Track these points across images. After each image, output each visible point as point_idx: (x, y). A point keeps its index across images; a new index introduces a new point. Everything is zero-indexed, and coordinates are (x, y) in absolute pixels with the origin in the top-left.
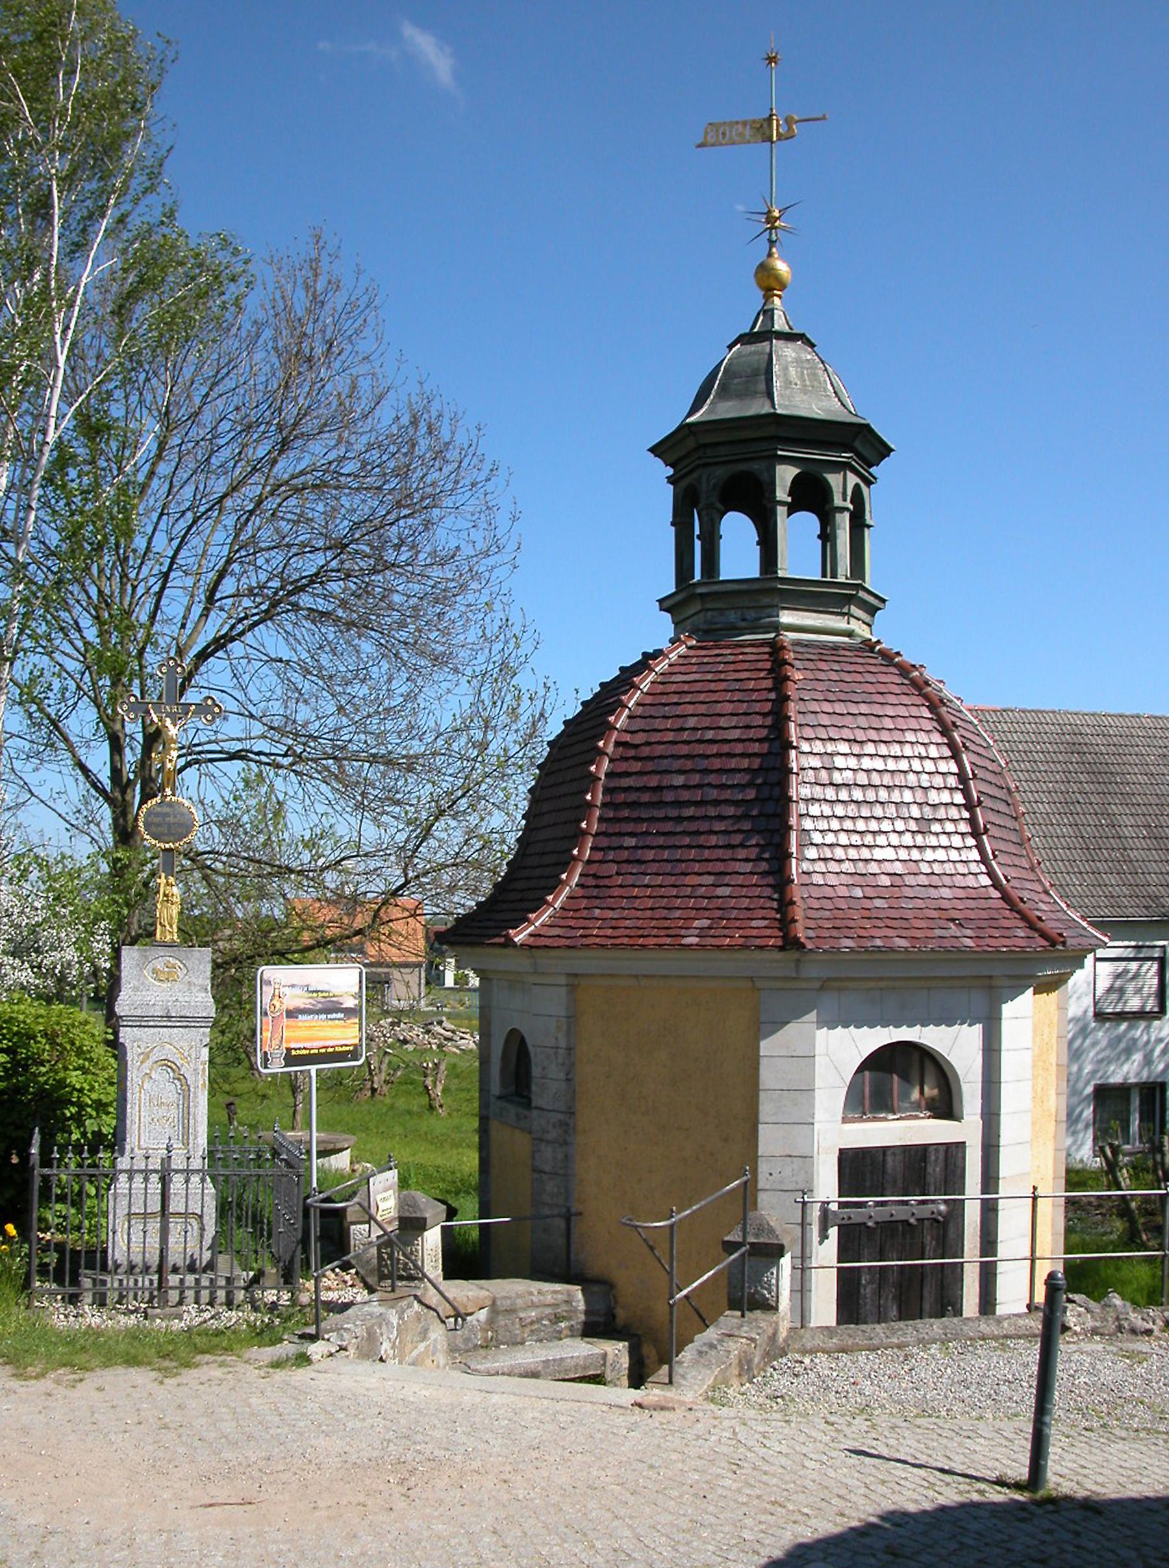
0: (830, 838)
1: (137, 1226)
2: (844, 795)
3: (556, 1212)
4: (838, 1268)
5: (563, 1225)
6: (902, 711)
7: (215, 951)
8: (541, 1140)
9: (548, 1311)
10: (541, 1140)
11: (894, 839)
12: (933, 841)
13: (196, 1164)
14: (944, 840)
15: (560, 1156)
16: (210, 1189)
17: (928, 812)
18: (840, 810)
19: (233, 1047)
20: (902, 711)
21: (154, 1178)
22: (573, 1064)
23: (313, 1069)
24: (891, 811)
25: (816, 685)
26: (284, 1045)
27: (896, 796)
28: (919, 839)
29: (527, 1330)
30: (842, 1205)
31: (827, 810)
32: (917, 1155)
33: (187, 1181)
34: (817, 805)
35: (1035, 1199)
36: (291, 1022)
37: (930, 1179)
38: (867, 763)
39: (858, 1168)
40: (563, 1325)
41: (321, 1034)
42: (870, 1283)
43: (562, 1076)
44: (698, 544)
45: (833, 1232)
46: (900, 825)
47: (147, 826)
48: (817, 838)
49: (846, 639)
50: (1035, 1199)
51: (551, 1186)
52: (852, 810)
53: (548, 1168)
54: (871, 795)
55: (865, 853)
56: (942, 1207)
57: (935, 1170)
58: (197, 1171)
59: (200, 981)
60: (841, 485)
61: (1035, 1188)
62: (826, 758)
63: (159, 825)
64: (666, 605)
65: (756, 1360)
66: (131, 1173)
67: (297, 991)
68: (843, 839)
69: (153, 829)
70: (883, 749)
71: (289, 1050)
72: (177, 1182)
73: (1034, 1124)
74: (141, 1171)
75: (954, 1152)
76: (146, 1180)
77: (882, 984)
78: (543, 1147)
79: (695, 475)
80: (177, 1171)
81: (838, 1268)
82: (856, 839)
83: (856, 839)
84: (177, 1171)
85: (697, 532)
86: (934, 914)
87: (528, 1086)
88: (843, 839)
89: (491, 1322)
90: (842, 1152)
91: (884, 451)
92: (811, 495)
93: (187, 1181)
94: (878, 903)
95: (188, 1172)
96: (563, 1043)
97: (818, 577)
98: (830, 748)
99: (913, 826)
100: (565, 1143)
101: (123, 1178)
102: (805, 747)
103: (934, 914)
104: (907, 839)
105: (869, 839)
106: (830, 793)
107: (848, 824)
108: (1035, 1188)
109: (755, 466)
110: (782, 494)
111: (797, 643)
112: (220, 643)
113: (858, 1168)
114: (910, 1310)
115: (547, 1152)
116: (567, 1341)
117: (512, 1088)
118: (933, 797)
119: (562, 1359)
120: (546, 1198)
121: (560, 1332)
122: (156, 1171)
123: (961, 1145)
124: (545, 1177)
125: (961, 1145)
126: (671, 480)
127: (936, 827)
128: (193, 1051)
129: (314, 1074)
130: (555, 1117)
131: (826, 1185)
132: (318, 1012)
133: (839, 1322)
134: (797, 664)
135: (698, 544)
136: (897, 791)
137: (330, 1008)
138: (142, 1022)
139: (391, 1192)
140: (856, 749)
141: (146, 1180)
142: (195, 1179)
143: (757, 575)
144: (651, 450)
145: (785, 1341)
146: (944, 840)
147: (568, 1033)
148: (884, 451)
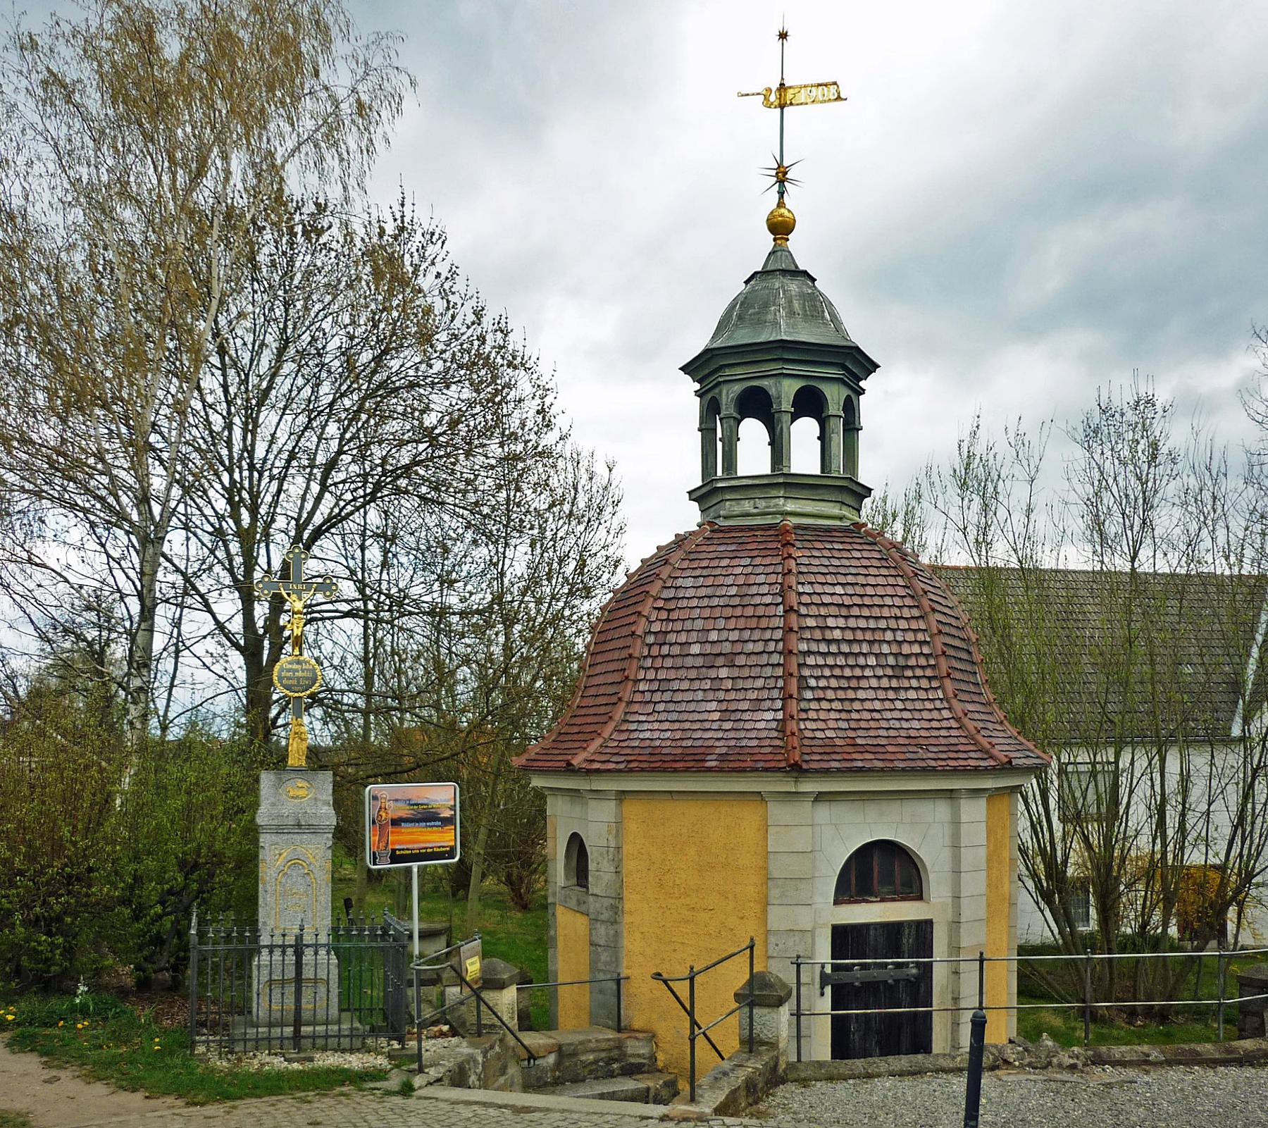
0: (823, 683)
2: (834, 649)
3: (609, 977)
5: (615, 987)
6: (881, 580)
7: (335, 775)
8: (597, 920)
9: (603, 1055)
10: (597, 920)
11: (874, 683)
12: (906, 684)
13: (323, 939)
14: (914, 683)
15: (612, 932)
16: (334, 960)
17: (902, 662)
18: (830, 661)
19: (347, 838)
20: (881, 580)
21: (290, 951)
22: (621, 860)
23: (415, 866)
24: (872, 661)
26: (390, 847)
27: (876, 649)
28: (894, 683)
29: (587, 1070)
30: (835, 968)
31: (821, 661)
32: (893, 930)
33: (316, 954)
34: (812, 657)
35: (981, 961)
36: (396, 829)
38: (852, 623)
39: (846, 939)
40: (615, 1066)
41: (422, 838)
44: (719, 445)
45: (828, 990)
46: (880, 672)
47: (280, 679)
48: (813, 683)
49: (838, 523)
50: (981, 961)
51: (604, 957)
52: (841, 661)
54: (856, 649)
55: (851, 694)
56: (914, 971)
57: (907, 940)
58: (324, 945)
59: (324, 797)
60: (834, 396)
61: (982, 954)
62: (820, 619)
63: (289, 678)
64: (694, 495)
65: (760, 1086)
66: (271, 948)
67: (399, 804)
68: (834, 683)
70: (866, 612)
71: (394, 851)
72: (309, 952)
73: (989, 905)
74: (280, 946)
75: (923, 929)
76: (284, 953)
79: (717, 391)
80: (308, 946)
82: (844, 683)
83: (844, 683)
84: (308, 946)
85: (719, 435)
87: (587, 878)
88: (834, 683)
89: (558, 1064)
91: (870, 367)
92: (809, 403)
93: (316, 954)
95: (316, 946)
96: (613, 844)
97: (818, 472)
98: (823, 611)
99: (889, 672)
100: (616, 922)
101: (265, 952)
102: (803, 610)
104: (885, 683)
105: (854, 683)
106: (823, 648)
107: (837, 672)
108: (982, 954)
109: (764, 383)
110: (787, 406)
111: (798, 527)
112: (333, 521)
113: (846, 939)
114: (890, 1048)
115: (602, 929)
116: (619, 1079)
117: (574, 881)
118: (906, 649)
120: (600, 966)
122: (291, 946)
123: (929, 923)
125: (929, 923)
126: (699, 394)
127: (909, 673)
128: (317, 852)
129: (415, 870)
130: (607, 902)
131: (823, 953)
132: (418, 821)
133: (834, 1057)
134: (798, 544)
135: (719, 445)
136: (876, 645)
137: (428, 817)
139: (476, 958)
140: (844, 612)
141: (284, 953)
142: (322, 952)
143: (769, 472)
145: (784, 1071)
146: (914, 683)
147: (617, 836)
148: (870, 367)
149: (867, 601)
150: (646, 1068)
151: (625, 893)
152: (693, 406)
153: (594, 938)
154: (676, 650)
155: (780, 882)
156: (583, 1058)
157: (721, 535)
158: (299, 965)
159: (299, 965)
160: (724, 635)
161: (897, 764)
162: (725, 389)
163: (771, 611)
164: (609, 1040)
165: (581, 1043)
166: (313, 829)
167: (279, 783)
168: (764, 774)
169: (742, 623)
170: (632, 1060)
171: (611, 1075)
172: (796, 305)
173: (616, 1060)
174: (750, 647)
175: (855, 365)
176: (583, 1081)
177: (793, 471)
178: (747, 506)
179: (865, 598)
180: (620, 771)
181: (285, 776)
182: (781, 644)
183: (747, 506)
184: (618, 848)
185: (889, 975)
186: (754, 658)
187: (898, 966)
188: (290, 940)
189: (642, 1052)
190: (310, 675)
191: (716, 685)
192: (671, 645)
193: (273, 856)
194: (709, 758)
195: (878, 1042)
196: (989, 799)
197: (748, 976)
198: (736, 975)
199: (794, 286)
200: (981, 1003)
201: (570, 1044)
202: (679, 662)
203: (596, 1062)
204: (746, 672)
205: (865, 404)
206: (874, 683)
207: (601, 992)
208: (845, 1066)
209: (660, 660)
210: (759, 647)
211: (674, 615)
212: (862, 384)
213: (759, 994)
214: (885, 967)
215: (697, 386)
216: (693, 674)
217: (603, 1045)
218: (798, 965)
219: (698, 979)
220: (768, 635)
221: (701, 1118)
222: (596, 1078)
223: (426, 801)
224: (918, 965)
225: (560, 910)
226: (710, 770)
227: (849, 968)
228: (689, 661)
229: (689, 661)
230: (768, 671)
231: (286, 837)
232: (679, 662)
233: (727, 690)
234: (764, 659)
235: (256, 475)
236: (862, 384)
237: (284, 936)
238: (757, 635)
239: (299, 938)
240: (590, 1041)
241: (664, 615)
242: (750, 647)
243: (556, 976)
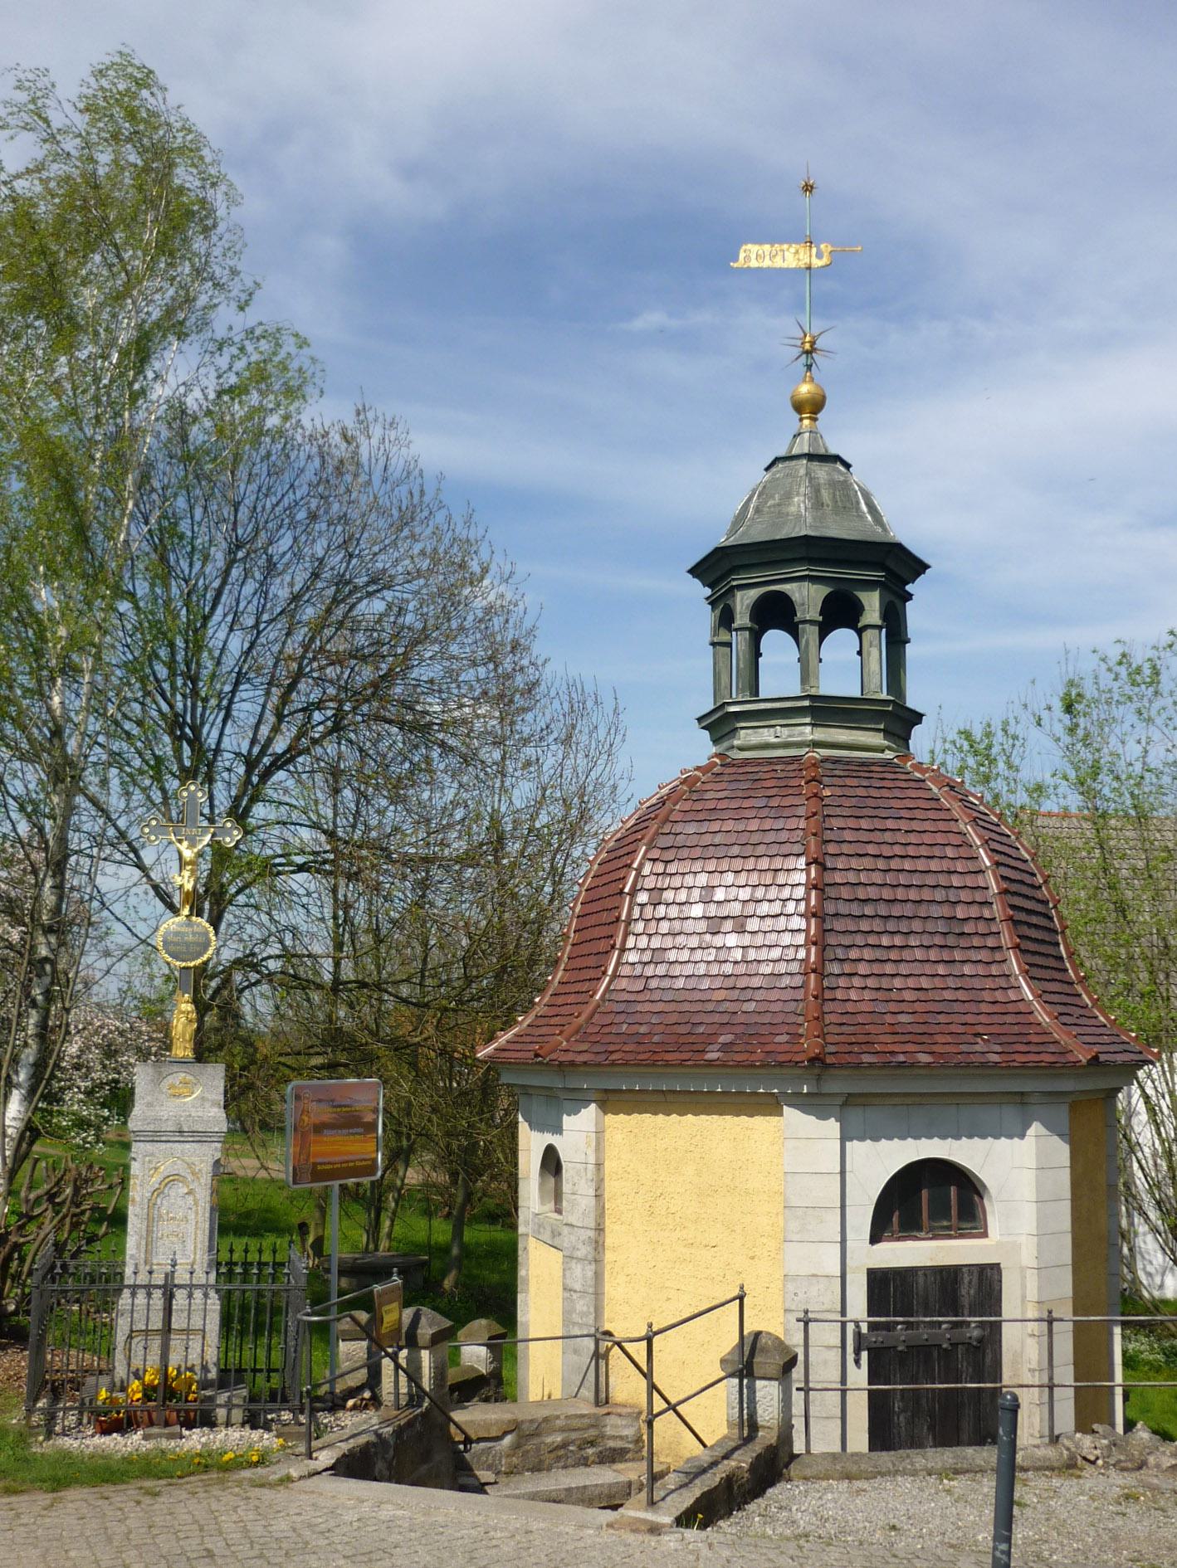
1: (138, 1343)
4: (870, 1391)
23: (336, 1184)
25: (843, 801)
30: (873, 1327)
32: (949, 1276)
35: (167, 1330)
37: (966, 1302)
42: (903, 1411)
43: (592, 1192)
45: (864, 1355)
52: (877, 925)
53: (578, 1287)
57: (967, 1292)
61: (1050, 1312)
69: (172, 948)
71: (315, 1164)
72: (180, 1297)
76: (149, 1295)
77: (909, 1101)
78: (573, 1264)
81: (870, 1391)
86: (961, 1029)
89: (516, 1446)
90: (996, 1267)
93: (190, 1296)
94: (903, 1018)
101: (126, 1293)
103: (961, 1029)
105: (893, 955)
108: (1050, 1312)
111: (826, 760)
114: (947, 1437)
118: (960, 912)
119: (585, 1487)
120: (576, 1318)
121: (586, 1459)
124: (575, 1296)
133: (870, 1450)
138: (155, 1137)
142: (198, 1294)
144: (691, 571)
149: (911, 851)
150: (629, 1456)
151: (607, 1223)
152: (706, 617)
153: (568, 1281)
154: (673, 912)
155: (800, 1212)
156: (549, 1440)
157: (734, 770)
158: (168, 1311)
159: (168, 1311)
160: (733, 892)
161: (973, 1058)
162: (739, 594)
163: (791, 863)
164: (583, 1416)
165: (546, 1420)
166: (600, 1133)
167: (158, 1080)
168: (777, 1071)
169: (754, 878)
170: (611, 1444)
171: (585, 1462)
172: (825, 495)
173: (592, 1443)
174: (764, 908)
175: (897, 567)
176: (549, 1469)
177: (822, 692)
178: (767, 736)
179: (910, 848)
180: (599, 1065)
181: (165, 1070)
182: (803, 904)
183: (767, 736)
184: (599, 1165)
185: (944, 1336)
186: (769, 921)
187: (955, 1325)
188: (159, 1279)
189: (626, 1432)
190: (202, 940)
191: (722, 956)
192: (668, 904)
193: (147, 1169)
194: (711, 1047)
195: (931, 1428)
196: (1073, 1107)
197: (736, 1340)
198: (723, 1336)
199: (822, 472)
200: (1051, 1378)
201: (532, 1421)
202: (677, 925)
203: (564, 1445)
204: (759, 940)
205: (914, 613)
206: (919, 954)
207: (575, 1351)
208: (885, 1458)
209: (654, 923)
210: (776, 908)
211: (672, 868)
212: (909, 588)
213: (750, 1360)
214: (936, 1326)
215: (708, 591)
216: (694, 942)
217: (575, 1423)
218: (806, 1324)
219: (656, 1339)
220: (786, 893)
221: (655, 1529)
222: (565, 1467)
223: (348, 1102)
224: (981, 1324)
225: (532, 1243)
226: (710, 1064)
227: (889, 1327)
228: (689, 926)
229: (689, 926)
230: (786, 939)
231: (164, 1146)
232: (677, 925)
233: (736, 963)
234: (781, 923)
235: (200, 704)
236: (909, 588)
237: (150, 1273)
238: (773, 893)
239: (169, 1276)
240: (558, 1417)
241: (660, 868)
242: (764, 908)
243: (527, 1330)
